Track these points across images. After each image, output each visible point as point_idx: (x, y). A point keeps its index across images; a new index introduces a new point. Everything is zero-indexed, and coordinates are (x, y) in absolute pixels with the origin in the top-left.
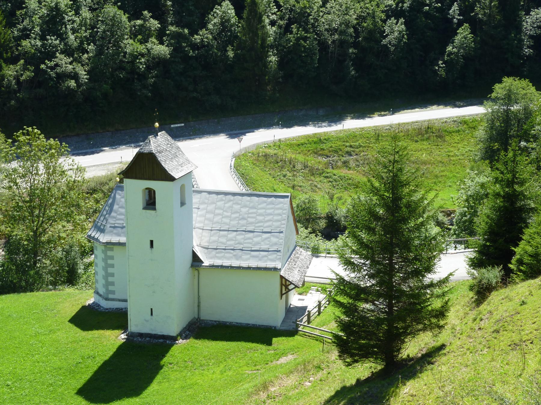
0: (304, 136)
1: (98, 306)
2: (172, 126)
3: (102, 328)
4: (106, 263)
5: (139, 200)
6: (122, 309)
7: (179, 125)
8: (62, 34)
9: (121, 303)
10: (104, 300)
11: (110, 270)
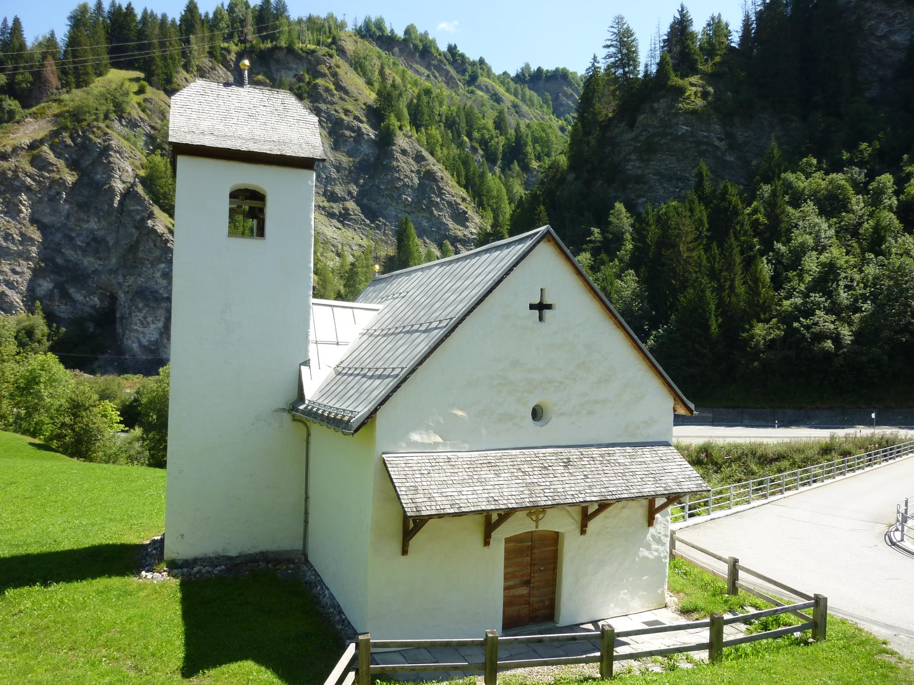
0: (167, 411)
3: (236, 660)
7: (592, 655)
8: (831, 292)
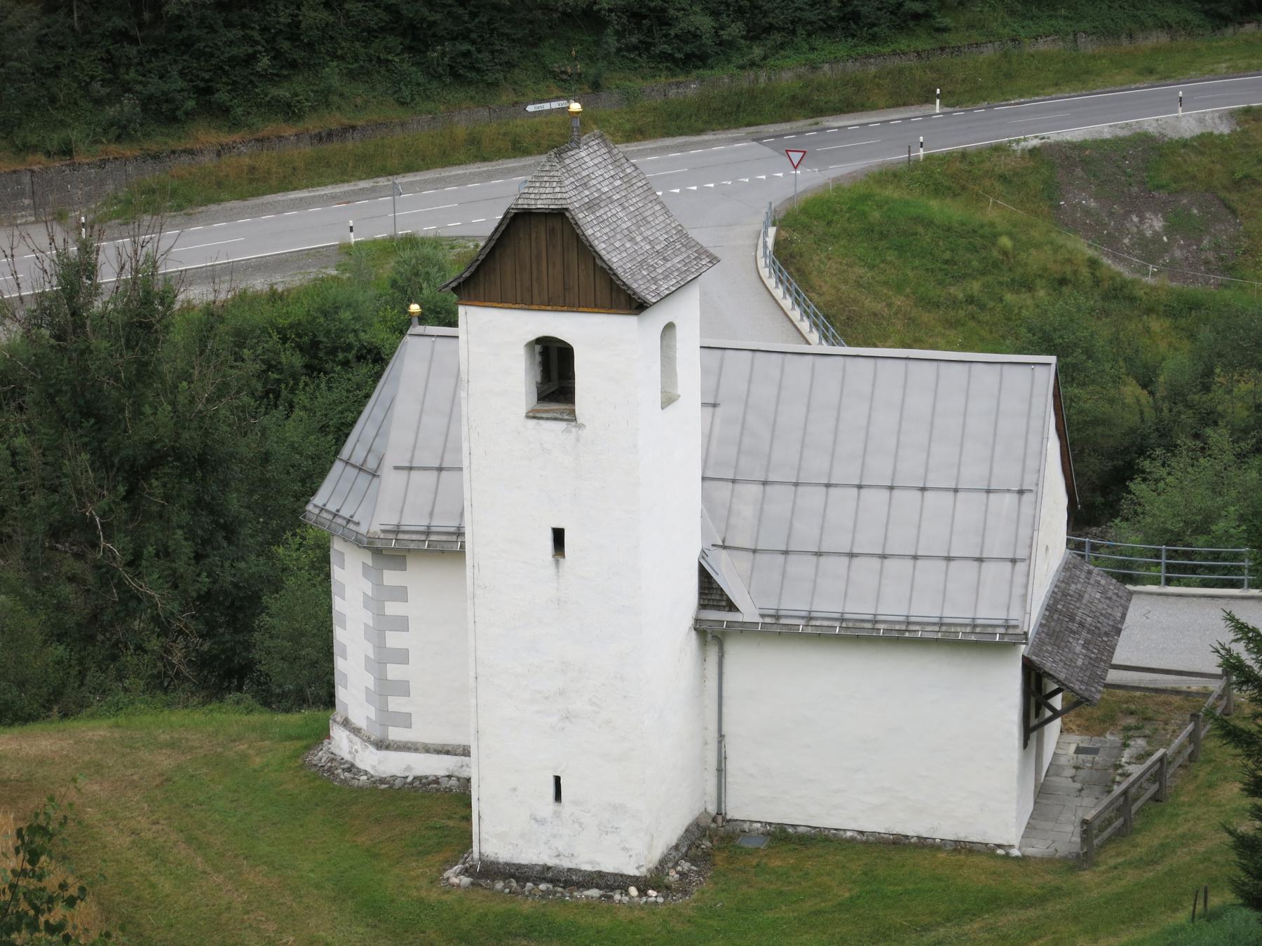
1: (349, 770)
2: (531, 108)
4: (380, 615)
5: (518, 378)
6: (436, 781)
9: (435, 757)
10: (372, 749)
11: (394, 640)
